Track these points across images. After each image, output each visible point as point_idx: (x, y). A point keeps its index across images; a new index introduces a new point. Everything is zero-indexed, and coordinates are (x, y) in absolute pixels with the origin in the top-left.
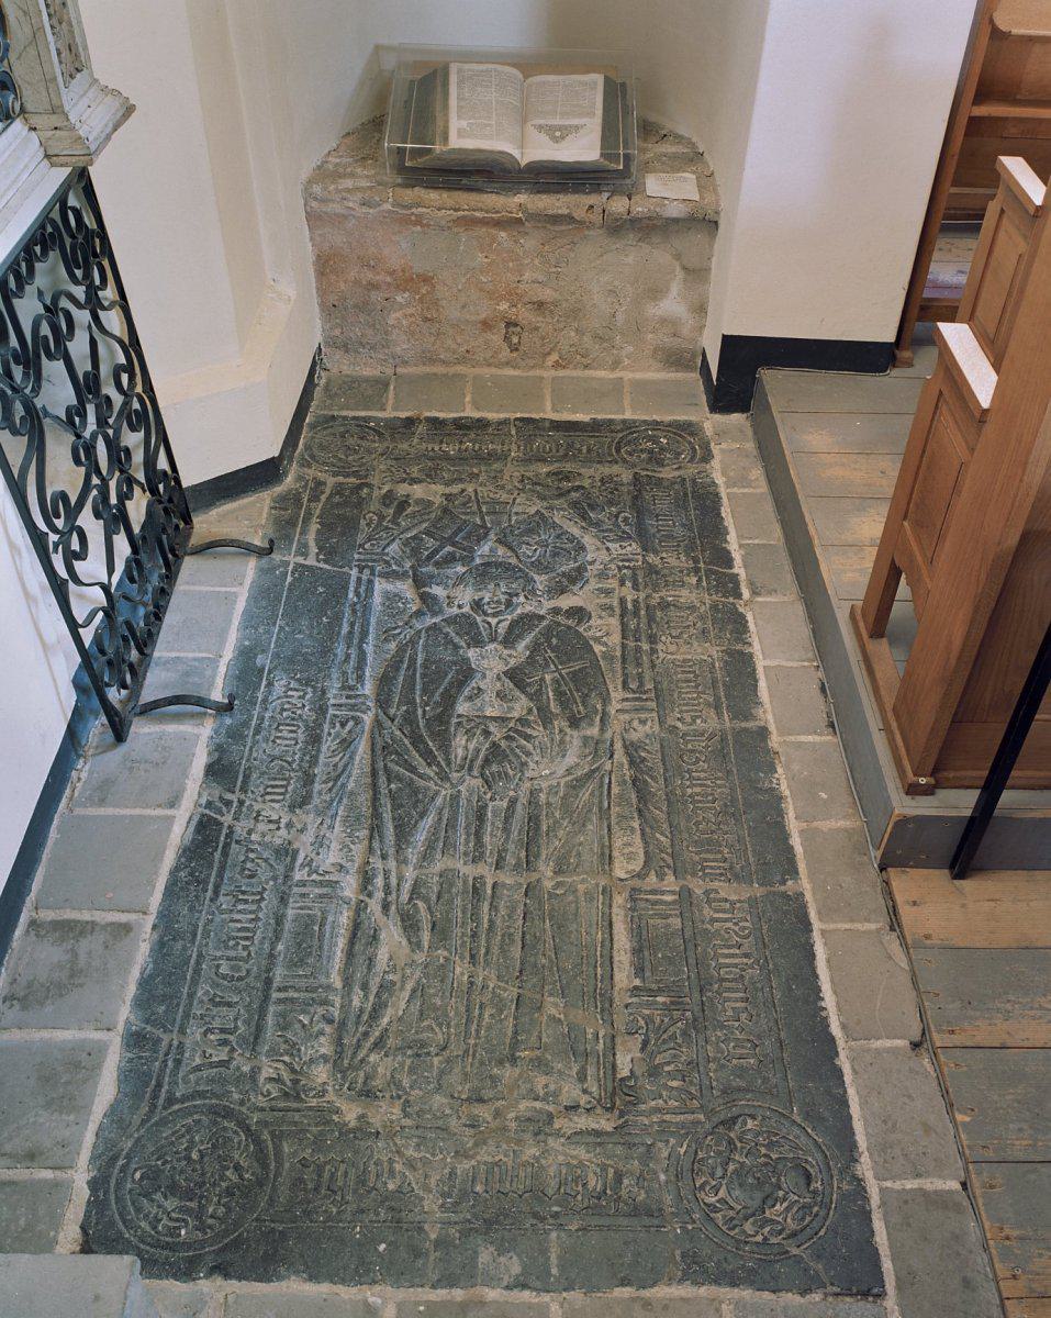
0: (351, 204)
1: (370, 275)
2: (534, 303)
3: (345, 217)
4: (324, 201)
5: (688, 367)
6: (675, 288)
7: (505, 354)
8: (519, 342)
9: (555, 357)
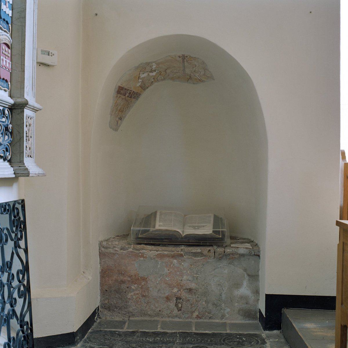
0: (117, 249)
1: (122, 278)
2: (188, 289)
3: (114, 254)
4: (106, 248)
5: (254, 318)
6: (245, 283)
7: (176, 312)
8: (182, 307)
9: (196, 313)
